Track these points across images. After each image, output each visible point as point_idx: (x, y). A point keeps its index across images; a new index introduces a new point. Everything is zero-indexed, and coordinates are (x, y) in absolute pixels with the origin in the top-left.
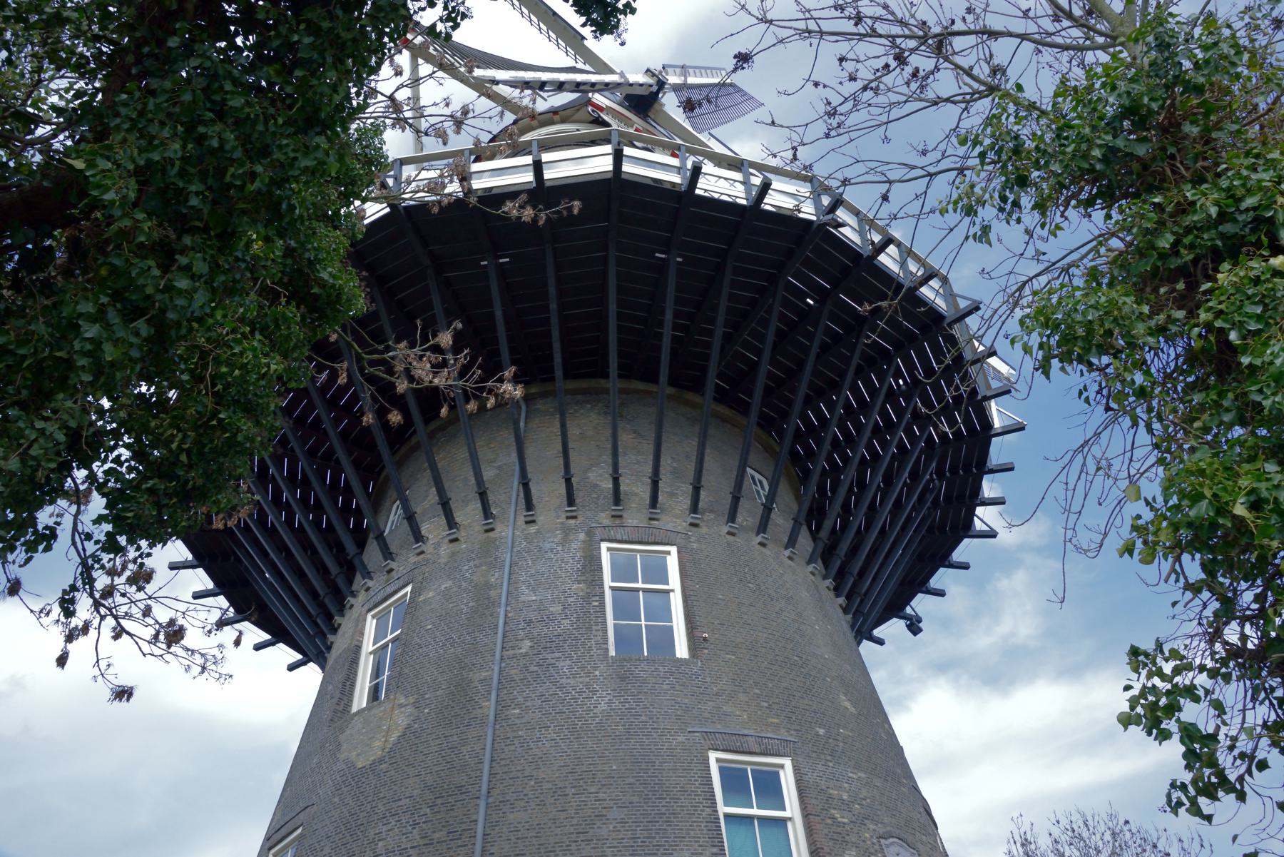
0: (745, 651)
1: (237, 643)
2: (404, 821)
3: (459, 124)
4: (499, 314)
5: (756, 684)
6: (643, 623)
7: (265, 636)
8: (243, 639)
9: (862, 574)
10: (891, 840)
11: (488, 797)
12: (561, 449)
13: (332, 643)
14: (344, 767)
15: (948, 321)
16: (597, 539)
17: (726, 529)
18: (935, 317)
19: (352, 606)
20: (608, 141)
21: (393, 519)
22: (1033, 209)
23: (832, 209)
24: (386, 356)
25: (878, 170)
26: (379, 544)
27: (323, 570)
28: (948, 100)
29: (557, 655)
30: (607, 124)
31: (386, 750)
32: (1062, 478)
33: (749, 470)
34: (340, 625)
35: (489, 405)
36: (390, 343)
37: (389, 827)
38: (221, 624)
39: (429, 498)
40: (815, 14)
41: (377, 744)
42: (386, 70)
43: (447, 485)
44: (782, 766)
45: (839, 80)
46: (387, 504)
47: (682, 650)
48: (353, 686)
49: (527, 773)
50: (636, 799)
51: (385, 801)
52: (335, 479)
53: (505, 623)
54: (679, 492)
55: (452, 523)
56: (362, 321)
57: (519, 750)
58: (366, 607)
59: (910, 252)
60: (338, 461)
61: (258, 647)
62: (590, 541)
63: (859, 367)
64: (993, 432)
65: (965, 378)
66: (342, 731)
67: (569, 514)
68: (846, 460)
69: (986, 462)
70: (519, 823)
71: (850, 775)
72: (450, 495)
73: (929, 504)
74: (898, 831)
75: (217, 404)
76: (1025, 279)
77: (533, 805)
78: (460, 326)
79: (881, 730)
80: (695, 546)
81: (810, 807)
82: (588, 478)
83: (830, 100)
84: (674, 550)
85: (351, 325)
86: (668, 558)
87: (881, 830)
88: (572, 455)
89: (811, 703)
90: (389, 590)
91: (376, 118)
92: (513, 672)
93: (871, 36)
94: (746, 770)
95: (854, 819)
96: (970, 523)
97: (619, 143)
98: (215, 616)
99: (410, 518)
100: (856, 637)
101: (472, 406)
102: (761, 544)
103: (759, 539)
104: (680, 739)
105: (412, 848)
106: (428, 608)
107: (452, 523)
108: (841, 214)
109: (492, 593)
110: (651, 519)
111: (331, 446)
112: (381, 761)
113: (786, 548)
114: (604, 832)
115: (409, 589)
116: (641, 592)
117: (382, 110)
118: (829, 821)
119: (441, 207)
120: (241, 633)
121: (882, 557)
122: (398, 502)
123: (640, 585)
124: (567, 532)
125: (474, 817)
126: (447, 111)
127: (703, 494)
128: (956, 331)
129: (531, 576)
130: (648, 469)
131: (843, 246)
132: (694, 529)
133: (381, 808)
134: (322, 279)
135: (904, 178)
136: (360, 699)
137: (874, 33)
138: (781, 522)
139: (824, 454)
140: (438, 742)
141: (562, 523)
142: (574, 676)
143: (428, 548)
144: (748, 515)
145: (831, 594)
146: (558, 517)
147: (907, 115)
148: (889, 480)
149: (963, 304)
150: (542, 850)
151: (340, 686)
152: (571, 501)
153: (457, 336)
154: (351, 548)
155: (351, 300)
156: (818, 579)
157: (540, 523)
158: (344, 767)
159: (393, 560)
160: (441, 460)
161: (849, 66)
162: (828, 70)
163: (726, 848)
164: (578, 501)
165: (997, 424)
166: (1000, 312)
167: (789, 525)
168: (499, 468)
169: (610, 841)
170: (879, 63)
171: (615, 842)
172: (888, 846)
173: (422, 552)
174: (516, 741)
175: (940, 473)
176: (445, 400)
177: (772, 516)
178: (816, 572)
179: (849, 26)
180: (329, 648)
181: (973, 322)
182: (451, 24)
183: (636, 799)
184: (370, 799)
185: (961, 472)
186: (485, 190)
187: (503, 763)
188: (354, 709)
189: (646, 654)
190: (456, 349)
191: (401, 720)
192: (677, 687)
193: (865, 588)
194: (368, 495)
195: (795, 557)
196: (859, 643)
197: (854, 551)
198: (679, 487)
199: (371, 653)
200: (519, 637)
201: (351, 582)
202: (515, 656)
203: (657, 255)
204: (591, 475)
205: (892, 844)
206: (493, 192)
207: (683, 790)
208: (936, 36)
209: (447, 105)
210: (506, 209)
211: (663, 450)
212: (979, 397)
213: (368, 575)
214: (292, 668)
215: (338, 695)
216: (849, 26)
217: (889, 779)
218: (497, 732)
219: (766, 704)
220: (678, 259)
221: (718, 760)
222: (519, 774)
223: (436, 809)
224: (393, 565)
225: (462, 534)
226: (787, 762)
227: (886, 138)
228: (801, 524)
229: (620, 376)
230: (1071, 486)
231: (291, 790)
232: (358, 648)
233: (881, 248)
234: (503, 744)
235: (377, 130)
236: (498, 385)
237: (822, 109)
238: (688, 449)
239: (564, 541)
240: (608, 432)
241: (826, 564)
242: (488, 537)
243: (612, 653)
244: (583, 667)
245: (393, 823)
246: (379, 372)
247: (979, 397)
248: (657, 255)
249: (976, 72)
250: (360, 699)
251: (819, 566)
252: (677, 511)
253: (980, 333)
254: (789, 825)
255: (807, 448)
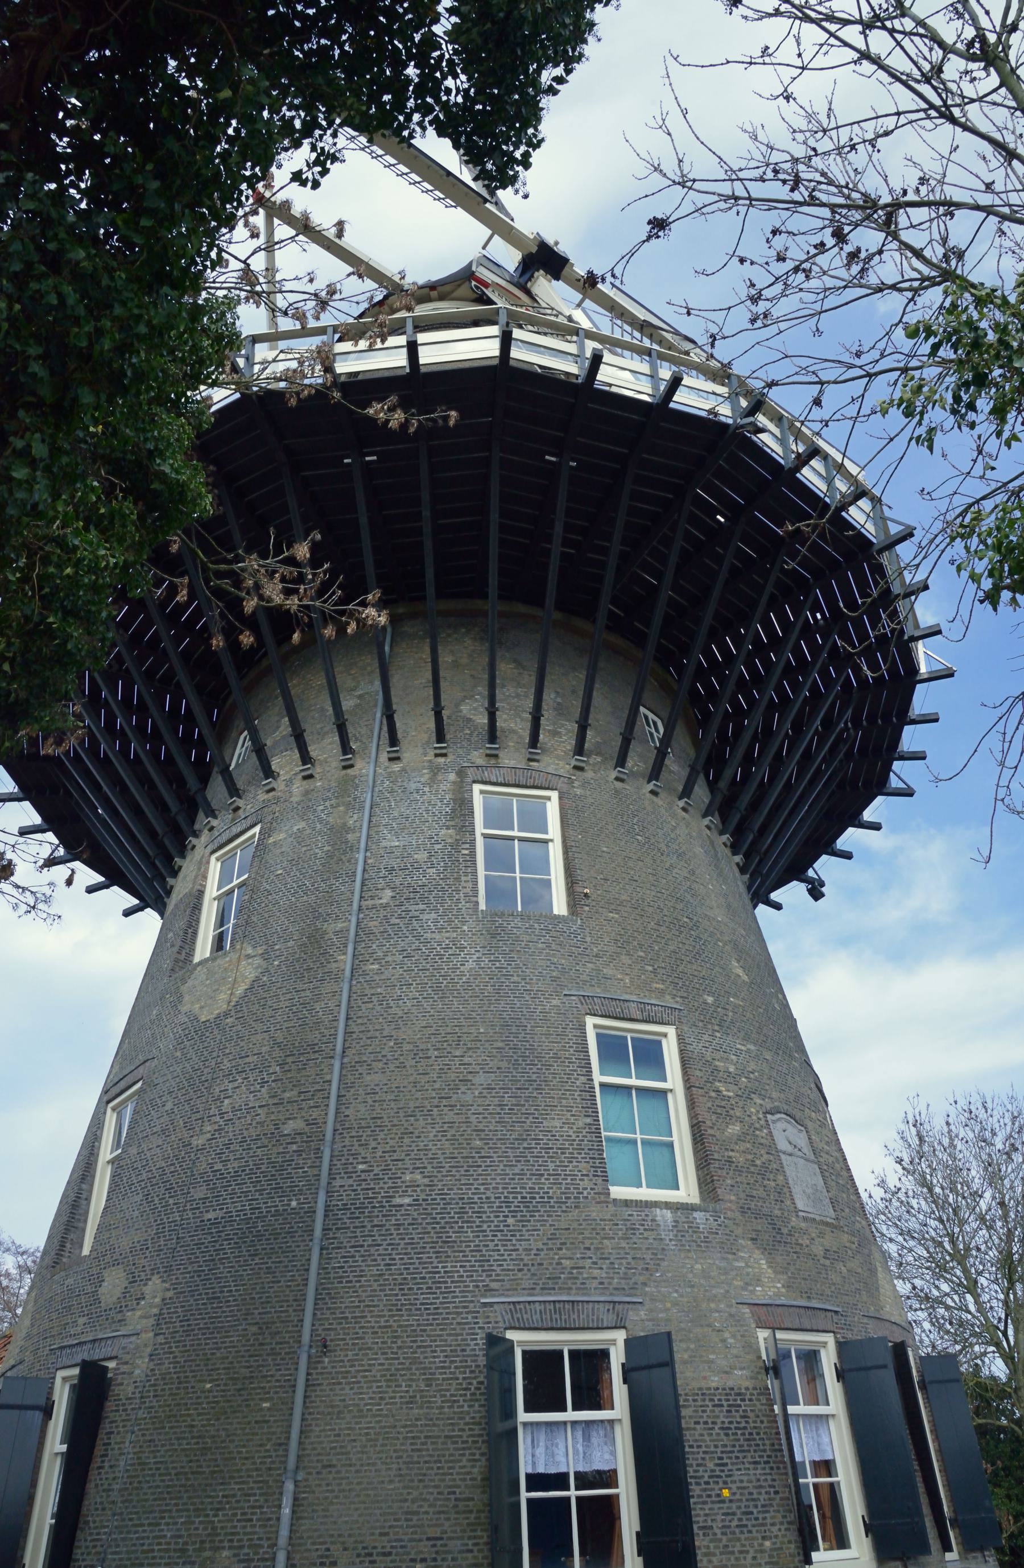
0: (630, 910)
1: (69, 882)
2: (251, 1079)
3: (323, 304)
4: (364, 520)
5: (641, 945)
6: (518, 875)
7: (99, 878)
8: (76, 877)
9: (763, 831)
10: (779, 1116)
11: (343, 1057)
12: (430, 678)
13: (172, 887)
14: (187, 1020)
15: (876, 548)
16: (469, 780)
17: (614, 774)
18: (862, 541)
19: (194, 847)
20: (493, 322)
21: (241, 750)
22: (990, 413)
23: (752, 411)
24: (234, 566)
25: (810, 369)
26: (224, 779)
27: (162, 806)
28: (894, 287)
29: (421, 907)
30: (491, 302)
31: (232, 1004)
32: (1000, 727)
33: (642, 709)
34: (180, 867)
35: (349, 631)
36: (240, 551)
37: (236, 1084)
38: (51, 862)
39: (281, 729)
40: (741, 175)
41: (223, 996)
42: (240, 232)
43: (301, 715)
44: (665, 1035)
45: (766, 260)
46: (234, 735)
47: (560, 906)
48: (195, 934)
49: (385, 1033)
50: (504, 1064)
51: (231, 1057)
52: (175, 705)
53: (364, 870)
54: (562, 730)
55: (306, 758)
56: (209, 524)
57: (378, 1008)
58: (210, 849)
59: (840, 468)
60: (178, 685)
61: (91, 890)
62: (462, 782)
63: (772, 598)
64: (918, 678)
65: (894, 615)
66: (184, 981)
67: (438, 751)
68: (751, 701)
69: (908, 711)
70: (378, 1085)
71: (738, 1046)
72: (304, 726)
73: (841, 755)
74: (786, 1107)
75: (44, 608)
76: (971, 500)
77: (391, 1066)
78: (319, 537)
79: (774, 1001)
80: (578, 791)
81: (693, 1079)
82: (461, 711)
83: (754, 281)
84: (554, 795)
85: (196, 528)
86: (549, 804)
87: (768, 1105)
88: (443, 685)
89: (700, 968)
90: (235, 830)
91: (229, 289)
92: (371, 924)
93: (809, 205)
94: (626, 1038)
95: (740, 1093)
96: (884, 779)
97: (508, 324)
98: (45, 852)
99: (260, 750)
100: (752, 900)
101: (329, 632)
102: (652, 792)
103: (651, 786)
104: (555, 1002)
105: (260, 1107)
106: (279, 851)
107: (306, 758)
108: (762, 420)
109: (350, 837)
110: (530, 760)
111: (171, 667)
112: (226, 1014)
113: (680, 798)
114: (468, 1098)
115: (257, 829)
116: (516, 841)
117: (234, 280)
118: (713, 1094)
119: (299, 400)
120: (73, 871)
121: (786, 812)
122: (246, 733)
123: (515, 833)
124: (435, 771)
125: (328, 1078)
126: (311, 288)
127: (590, 733)
128: (885, 559)
129: (394, 819)
130: (529, 704)
131: (760, 454)
132: (578, 773)
133: (227, 1064)
134: (163, 473)
135: (840, 379)
136: (203, 948)
137: (813, 201)
138: (676, 768)
139: (728, 693)
140: (288, 996)
141: (430, 761)
142: (440, 930)
143: (280, 785)
144: (638, 761)
145: (728, 851)
146: (425, 755)
147: (847, 304)
148: (799, 727)
149: (894, 529)
150: (401, 1114)
151: (181, 933)
152: (440, 737)
153: (314, 548)
154: (192, 783)
155: (195, 500)
156: (714, 835)
157: (405, 761)
158: (187, 1020)
159: (240, 797)
160: (295, 687)
161: (779, 242)
162: (755, 247)
163: (601, 1118)
164: (448, 737)
165: (923, 669)
166: (937, 541)
167: (684, 773)
168: (360, 697)
169: (475, 1107)
170: (816, 240)
171: (481, 1108)
172: (774, 1122)
173: (273, 790)
174: (374, 999)
175: (856, 721)
176: (298, 625)
177: (667, 762)
178: (713, 826)
179: (782, 192)
180: (169, 892)
181: (905, 551)
182: (319, 169)
183: (504, 1064)
184: (215, 1054)
185: (880, 721)
186: (350, 374)
187: (359, 1021)
188: (197, 959)
189: (520, 909)
190: (315, 562)
191: (249, 971)
192: (554, 946)
193: (766, 846)
194: (213, 725)
195: (690, 808)
196: (755, 906)
197: (755, 806)
198: (563, 725)
199: (215, 899)
200: (380, 886)
201: (193, 822)
202: (374, 907)
203: (547, 457)
204: (465, 708)
205: (779, 1119)
206: (360, 377)
207: (556, 1057)
208: (886, 206)
209: (311, 281)
210: (371, 411)
211: (546, 683)
212: (906, 637)
213: (212, 813)
214: (128, 913)
215: (179, 943)
216: (782, 192)
217: (781, 1052)
218: (354, 988)
219: (650, 968)
220: (571, 464)
221: (595, 1026)
222: (377, 1034)
223: (287, 1067)
224: (240, 803)
225: (317, 771)
226: (671, 1031)
227: (818, 330)
228: (698, 773)
229: (501, 597)
230: (1008, 738)
231: (129, 1043)
232: (201, 893)
233: (803, 460)
234: (360, 1002)
235: (231, 303)
236: (360, 609)
237: (744, 292)
238: (574, 683)
239: (433, 781)
240: (485, 660)
241: (724, 820)
242: (346, 775)
243: (482, 906)
244: (450, 921)
245: (240, 1081)
246: (225, 584)
247: (906, 637)
248: (547, 457)
249: (927, 253)
250: (203, 948)
251: (716, 820)
252: (559, 752)
253: (916, 562)
254: (670, 1096)
255: (709, 687)
